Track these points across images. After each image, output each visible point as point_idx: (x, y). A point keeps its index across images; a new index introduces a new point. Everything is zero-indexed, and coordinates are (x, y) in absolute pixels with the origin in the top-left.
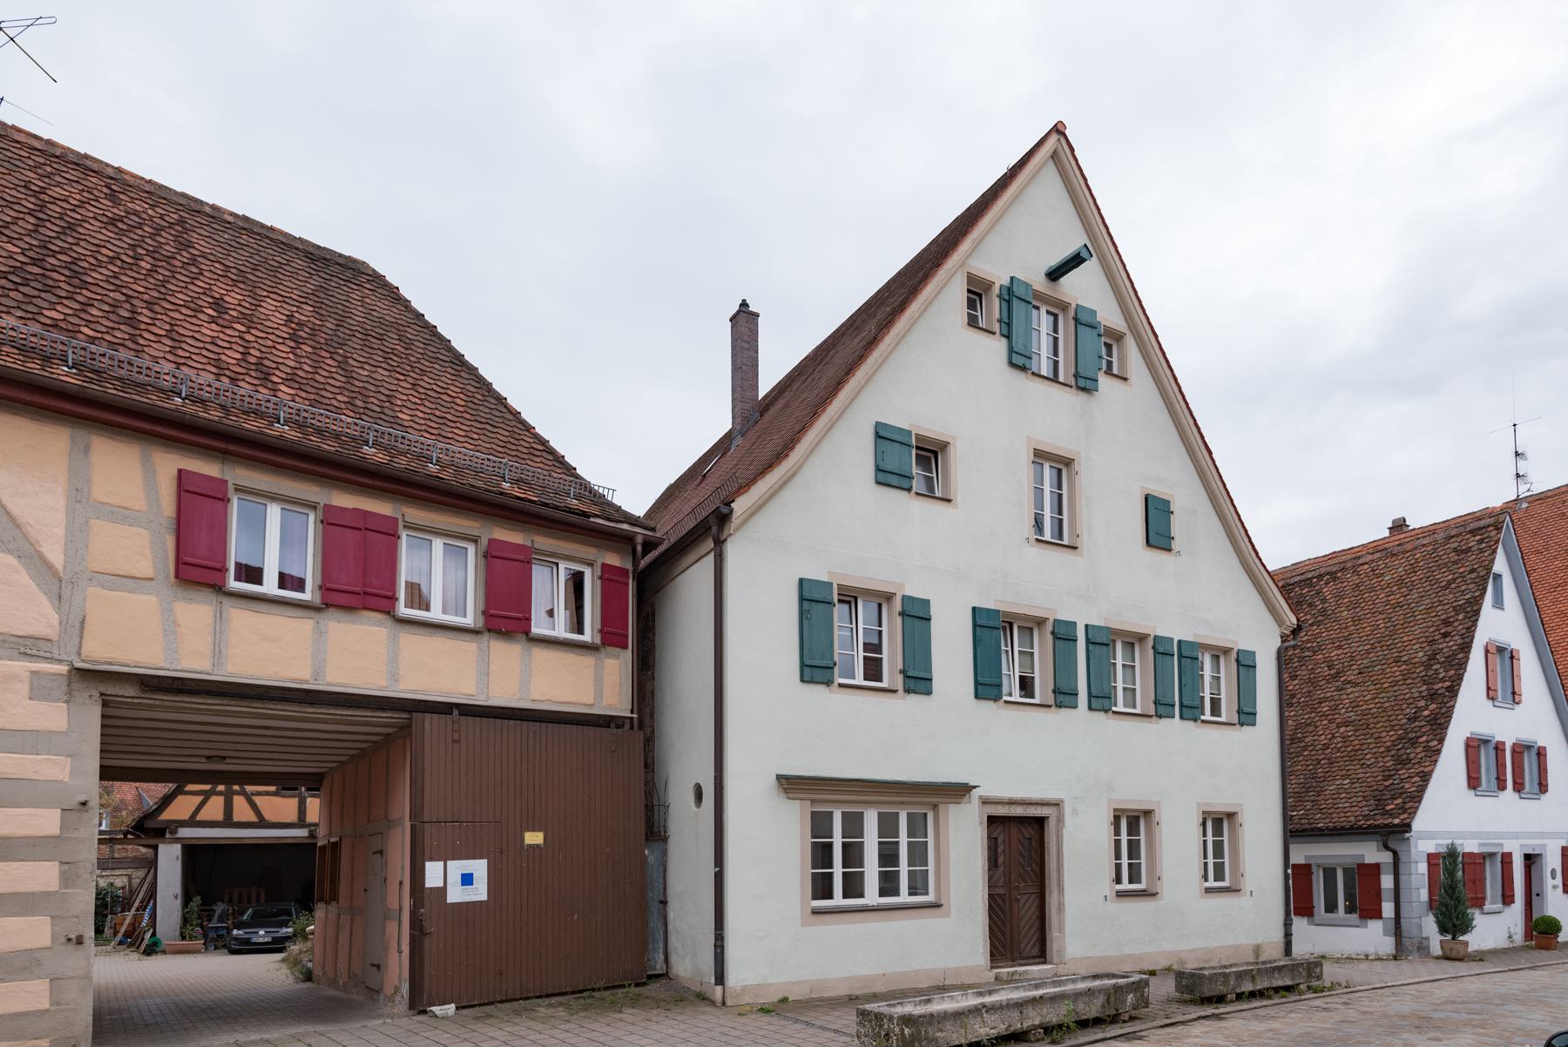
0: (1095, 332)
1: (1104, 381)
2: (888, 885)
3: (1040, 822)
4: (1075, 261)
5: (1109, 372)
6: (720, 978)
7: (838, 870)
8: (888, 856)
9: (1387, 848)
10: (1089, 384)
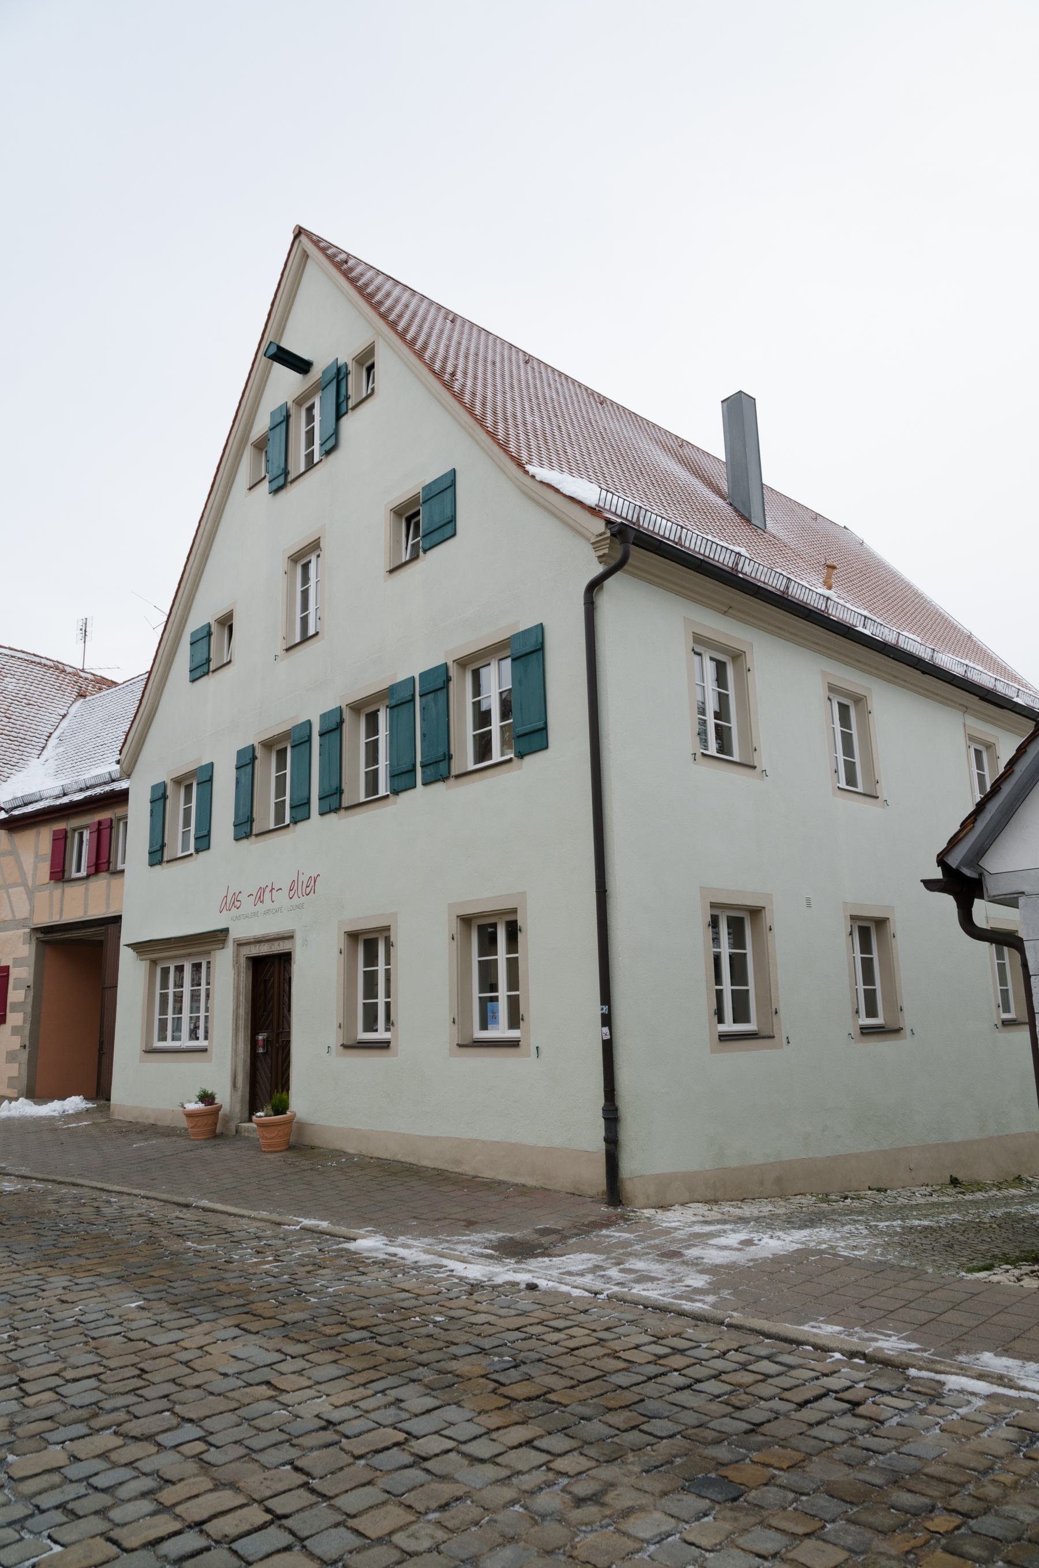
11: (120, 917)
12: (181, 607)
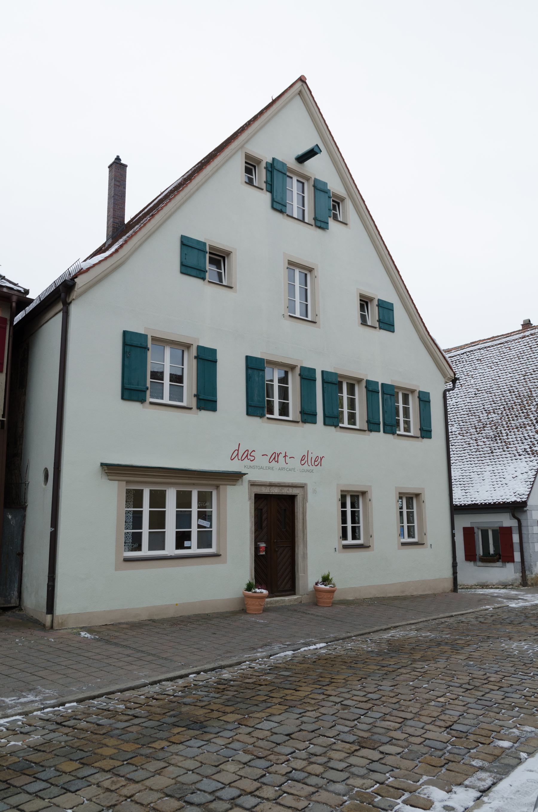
0: (327, 195)
1: (331, 223)
2: (182, 539)
3: (292, 498)
4: (311, 153)
5: (335, 218)
6: (50, 608)
8: (183, 519)
9: (515, 517)
10: (323, 225)
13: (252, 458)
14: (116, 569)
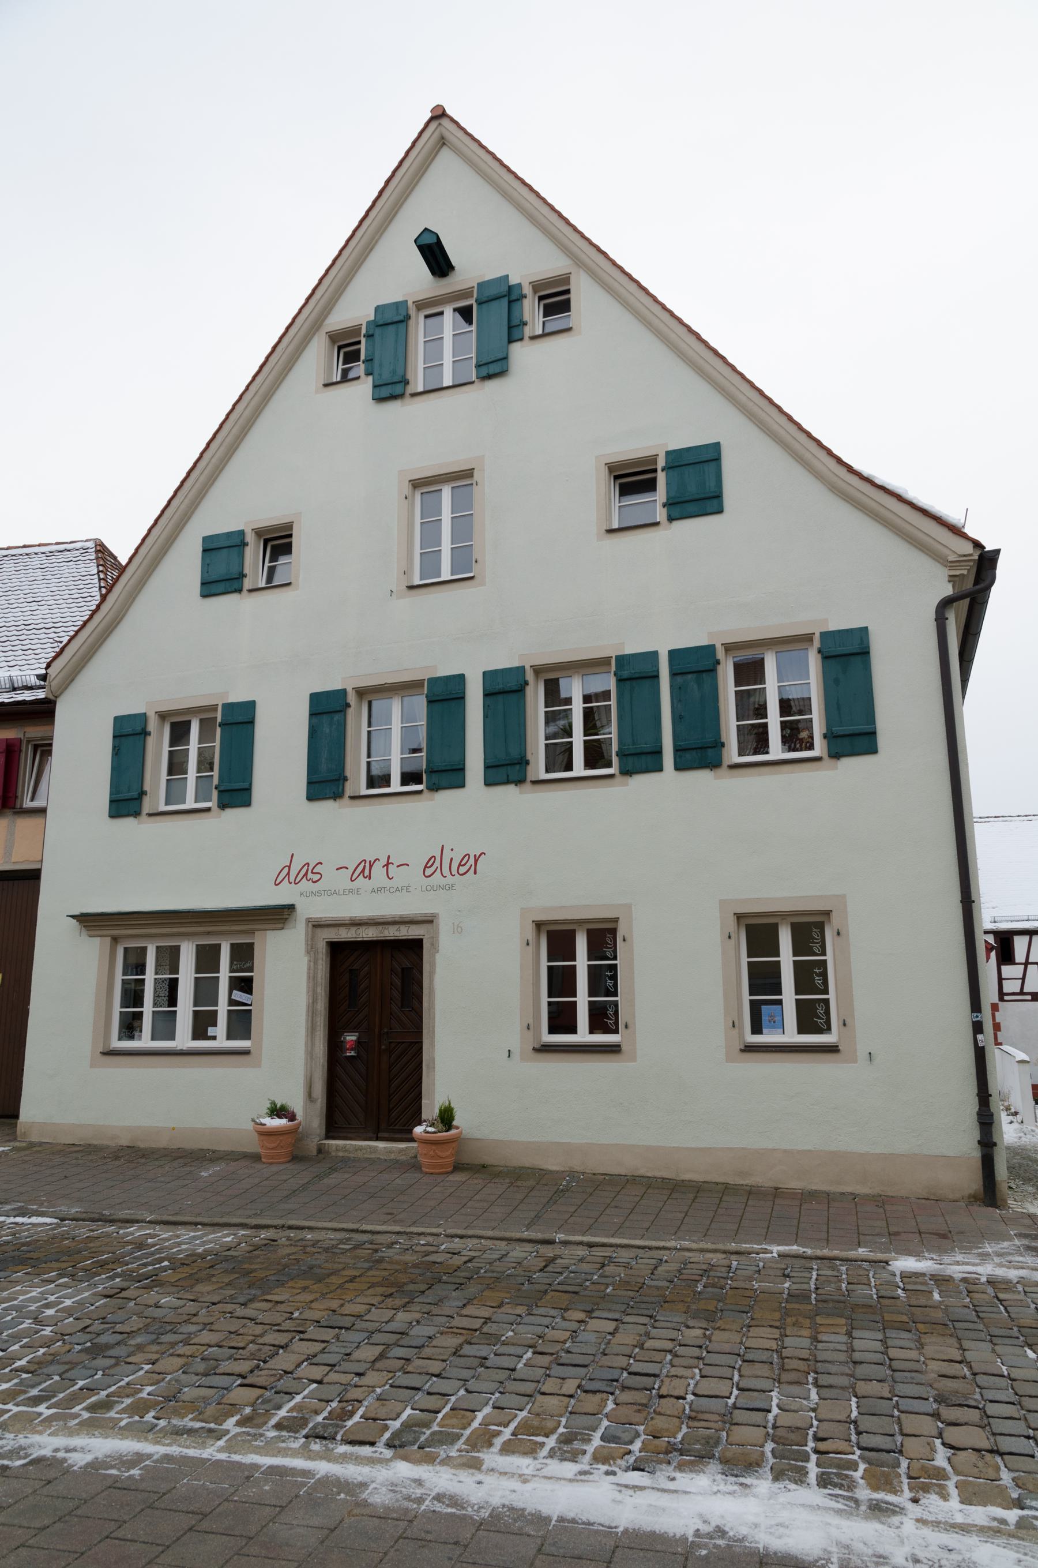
7: (582, 999)
8: (205, 991)
11: (34, 876)
12: (187, 501)
13: (316, 877)
14: (92, 1066)
